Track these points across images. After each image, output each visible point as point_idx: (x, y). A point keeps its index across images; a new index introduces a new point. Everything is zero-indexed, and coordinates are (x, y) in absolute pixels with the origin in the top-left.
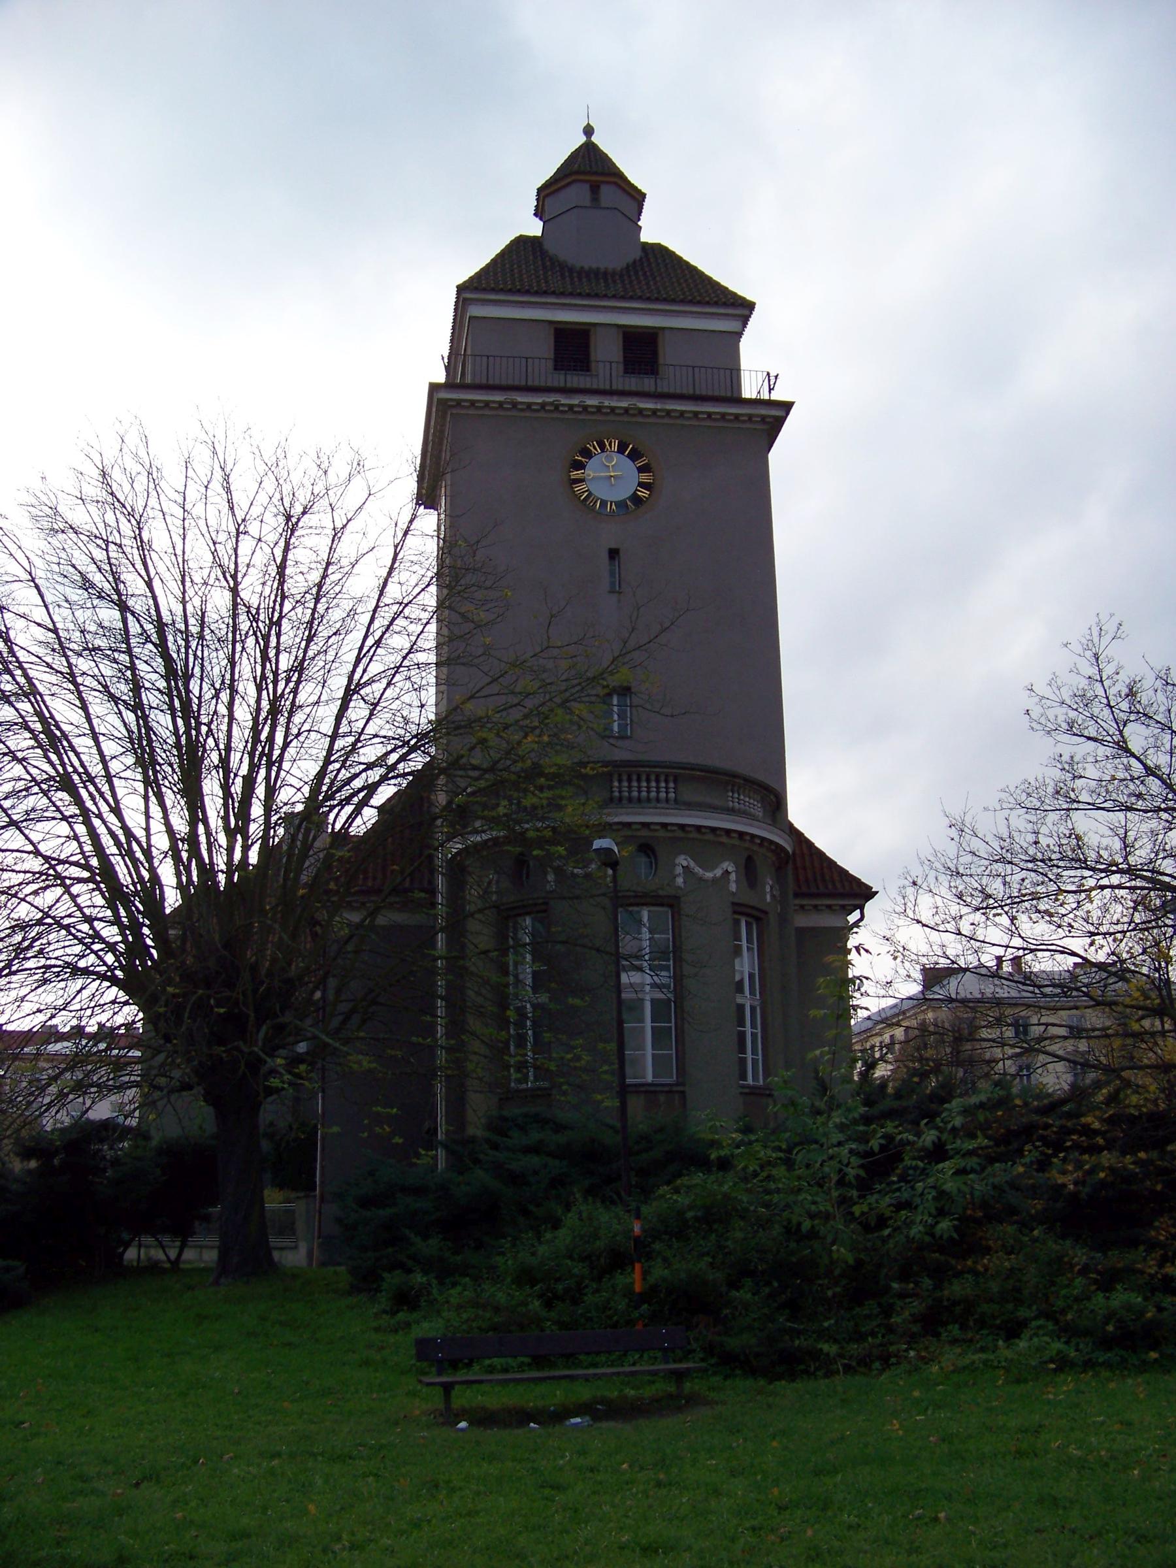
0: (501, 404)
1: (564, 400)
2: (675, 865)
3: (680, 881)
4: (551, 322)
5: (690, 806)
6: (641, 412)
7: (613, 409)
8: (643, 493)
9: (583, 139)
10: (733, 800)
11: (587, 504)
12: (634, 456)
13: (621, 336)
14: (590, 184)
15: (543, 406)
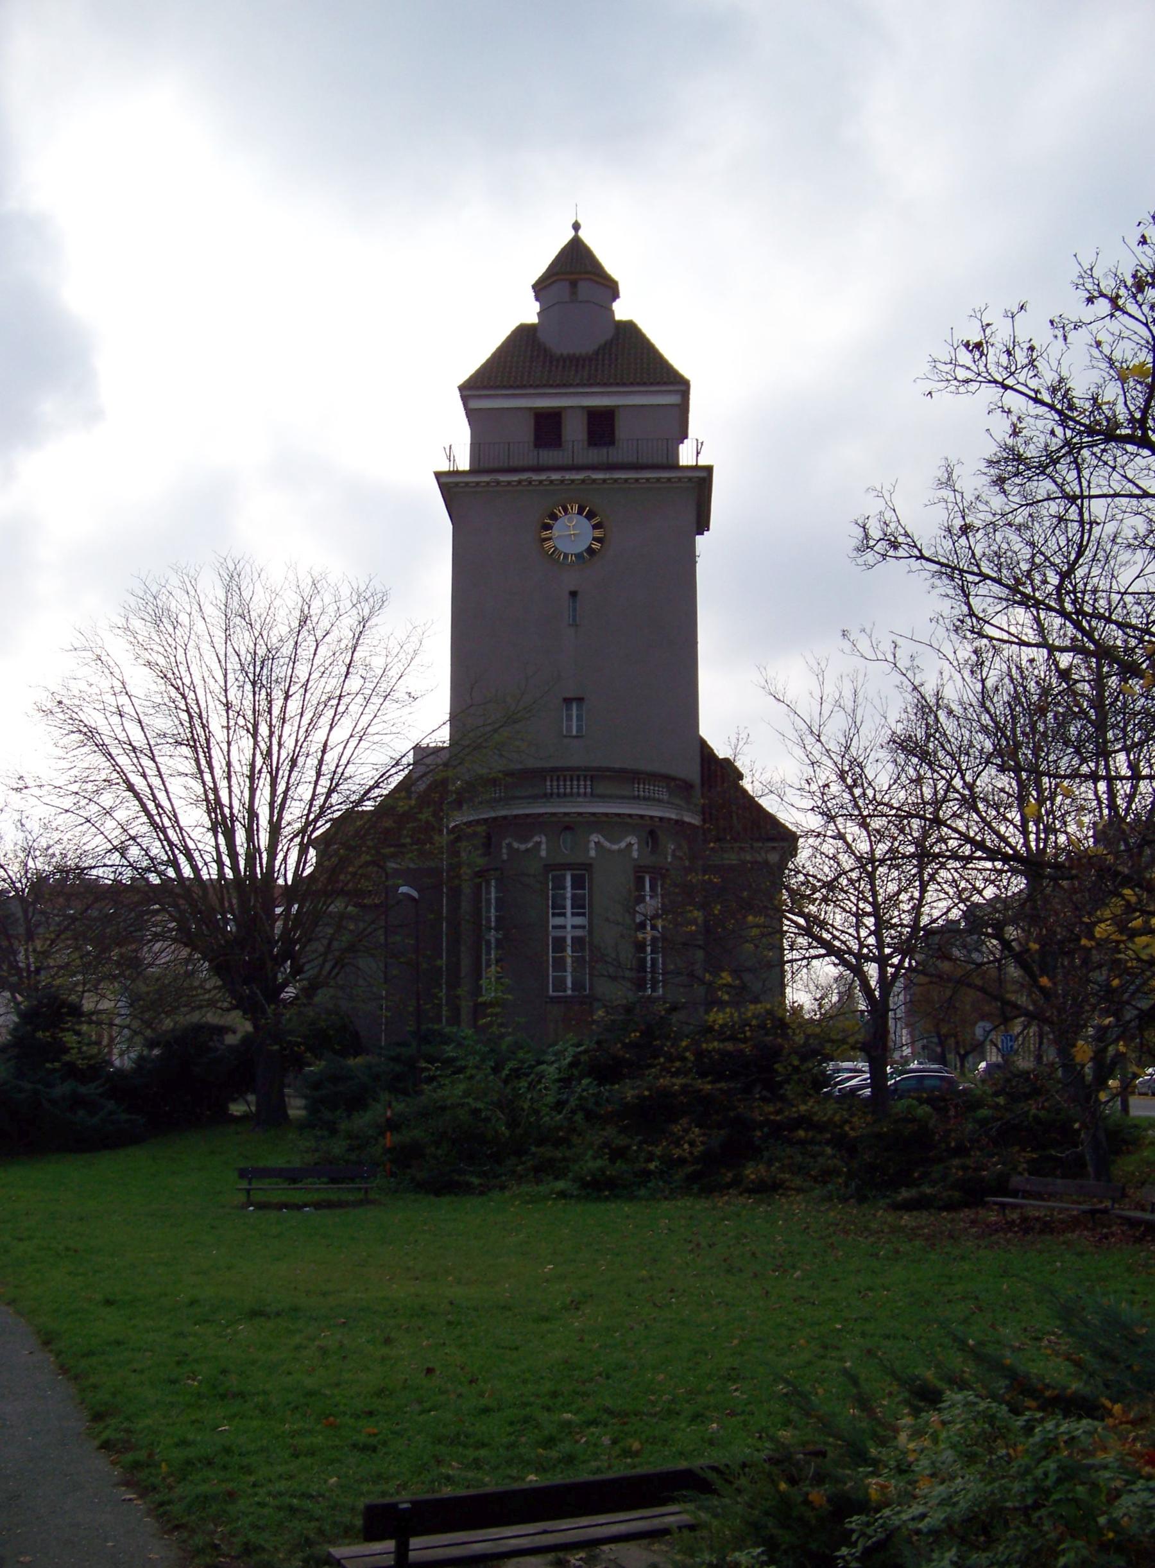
0: (488, 483)
1: (535, 477)
2: (589, 841)
3: (593, 853)
4: (531, 409)
5: (602, 797)
6: (594, 481)
7: (573, 481)
8: (596, 546)
9: (572, 233)
10: (641, 790)
11: (554, 558)
12: (590, 516)
13: (585, 417)
14: (576, 277)
15: (520, 482)
